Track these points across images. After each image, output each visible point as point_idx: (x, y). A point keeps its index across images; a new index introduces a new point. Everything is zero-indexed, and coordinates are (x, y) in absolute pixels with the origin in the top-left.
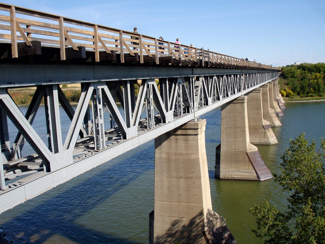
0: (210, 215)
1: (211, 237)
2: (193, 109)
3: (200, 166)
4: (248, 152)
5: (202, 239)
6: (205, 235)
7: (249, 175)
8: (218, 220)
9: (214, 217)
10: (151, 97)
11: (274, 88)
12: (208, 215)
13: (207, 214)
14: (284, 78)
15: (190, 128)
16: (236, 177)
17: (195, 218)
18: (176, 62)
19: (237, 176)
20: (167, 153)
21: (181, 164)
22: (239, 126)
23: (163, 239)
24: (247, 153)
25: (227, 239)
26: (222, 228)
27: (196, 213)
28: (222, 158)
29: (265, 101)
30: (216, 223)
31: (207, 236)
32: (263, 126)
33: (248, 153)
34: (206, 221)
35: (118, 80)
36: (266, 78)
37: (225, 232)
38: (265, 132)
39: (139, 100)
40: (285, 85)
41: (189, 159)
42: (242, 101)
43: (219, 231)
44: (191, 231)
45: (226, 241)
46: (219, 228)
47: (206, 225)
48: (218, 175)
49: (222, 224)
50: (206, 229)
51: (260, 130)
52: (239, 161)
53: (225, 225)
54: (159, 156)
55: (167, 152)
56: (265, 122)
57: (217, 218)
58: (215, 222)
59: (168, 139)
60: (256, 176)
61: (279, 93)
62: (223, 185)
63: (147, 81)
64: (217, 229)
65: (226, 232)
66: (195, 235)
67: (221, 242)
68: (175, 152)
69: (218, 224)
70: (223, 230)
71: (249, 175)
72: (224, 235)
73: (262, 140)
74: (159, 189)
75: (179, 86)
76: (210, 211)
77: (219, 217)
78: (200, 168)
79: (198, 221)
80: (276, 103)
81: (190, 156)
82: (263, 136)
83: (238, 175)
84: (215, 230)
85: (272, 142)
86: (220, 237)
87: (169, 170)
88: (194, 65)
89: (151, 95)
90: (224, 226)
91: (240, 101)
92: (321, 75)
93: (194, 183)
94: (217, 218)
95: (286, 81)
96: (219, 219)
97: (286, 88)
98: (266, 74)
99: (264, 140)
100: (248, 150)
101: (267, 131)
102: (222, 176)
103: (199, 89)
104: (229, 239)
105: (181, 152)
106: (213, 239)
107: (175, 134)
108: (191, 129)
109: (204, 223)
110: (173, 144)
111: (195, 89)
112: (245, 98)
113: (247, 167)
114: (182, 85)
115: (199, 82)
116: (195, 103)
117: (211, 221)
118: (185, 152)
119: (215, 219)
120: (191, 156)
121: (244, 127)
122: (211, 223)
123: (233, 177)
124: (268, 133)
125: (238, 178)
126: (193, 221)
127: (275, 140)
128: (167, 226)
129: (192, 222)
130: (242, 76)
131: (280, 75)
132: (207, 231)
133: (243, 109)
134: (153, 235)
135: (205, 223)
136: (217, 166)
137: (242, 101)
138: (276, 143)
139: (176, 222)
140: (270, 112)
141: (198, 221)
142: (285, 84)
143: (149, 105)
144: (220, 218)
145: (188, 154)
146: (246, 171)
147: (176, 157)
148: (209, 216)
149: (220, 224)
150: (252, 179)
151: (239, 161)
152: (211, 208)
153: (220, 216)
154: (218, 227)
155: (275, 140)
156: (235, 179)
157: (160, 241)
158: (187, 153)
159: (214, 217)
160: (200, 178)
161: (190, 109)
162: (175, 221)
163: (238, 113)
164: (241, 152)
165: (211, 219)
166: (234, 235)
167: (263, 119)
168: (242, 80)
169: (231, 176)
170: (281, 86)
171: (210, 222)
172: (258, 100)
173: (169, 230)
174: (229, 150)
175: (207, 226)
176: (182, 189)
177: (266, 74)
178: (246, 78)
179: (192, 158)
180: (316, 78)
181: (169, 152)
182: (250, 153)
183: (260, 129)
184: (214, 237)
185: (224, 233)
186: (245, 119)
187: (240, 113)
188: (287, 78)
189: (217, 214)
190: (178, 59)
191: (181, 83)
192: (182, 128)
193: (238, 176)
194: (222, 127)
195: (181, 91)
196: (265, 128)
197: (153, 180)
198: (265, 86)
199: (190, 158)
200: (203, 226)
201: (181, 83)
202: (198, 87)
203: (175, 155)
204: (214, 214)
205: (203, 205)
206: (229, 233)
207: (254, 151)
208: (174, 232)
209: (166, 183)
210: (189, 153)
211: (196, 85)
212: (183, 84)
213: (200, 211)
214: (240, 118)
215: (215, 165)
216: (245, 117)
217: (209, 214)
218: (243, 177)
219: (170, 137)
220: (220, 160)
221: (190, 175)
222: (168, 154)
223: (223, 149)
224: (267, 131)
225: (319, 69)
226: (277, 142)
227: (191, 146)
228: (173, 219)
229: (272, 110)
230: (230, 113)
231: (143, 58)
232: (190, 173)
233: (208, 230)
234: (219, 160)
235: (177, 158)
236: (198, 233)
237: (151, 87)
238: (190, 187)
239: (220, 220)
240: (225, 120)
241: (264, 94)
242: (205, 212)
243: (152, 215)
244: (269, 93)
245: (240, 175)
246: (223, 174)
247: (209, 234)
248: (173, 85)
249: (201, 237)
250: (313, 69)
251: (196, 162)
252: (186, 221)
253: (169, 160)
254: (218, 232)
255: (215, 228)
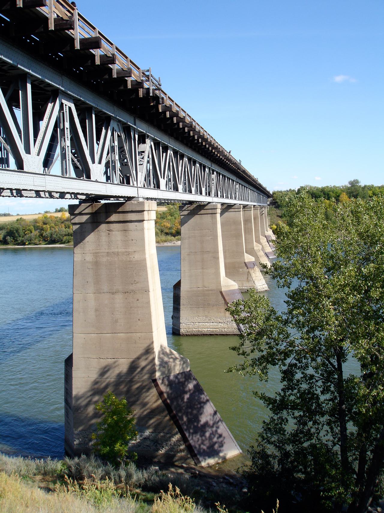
0: (163, 354)
1: (167, 388)
2: (135, 181)
3: (147, 272)
4: (223, 290)
5: (152, 392)
6: (157, 386)
7: (225, 326)
8: (178, 362)
9: (170, 357)
10: (67, 125)
11: (262, 219)
12: (161, 354)
13: (159, 352)
14: (276, 207)
15: (131, 210)
16: (205, 330)
17: (139, 358)
18: (108, 60)
19: (206, 330)
20: (94, 253)
21: (117, 271)
22: (208, 250)
23: (85, 400)
24: (221, 293)
25: (192, 392)
26: (184, 375)
27: (140, 351)
28: (182, 301)
29: (248, 231)
30: (174, 366)
31: (160, 386)
32: (245, 263)
33: (223, 292)
34: (157, 362)
35: (12, 63)
36: (249, 197)
37: (188, 381)
38: (249, 272)
39: (47, 122)
40: (278, 218)
41: (129, 261)
42: (213, 211)
43: (179, 380)
44: (131, 381)
45: (191, 395)
46: (178, 374)
47: (157, 368)
48: (178, 328)
49: (183, 368)
50: (158, 374)
51: (241, 270)
52: (209, 304)
53: (188, 369)
54: (80, 259)
55: (94, 251)
56: (249, 258)
57: (175, 359)
58: (173, 364)
59: (95, 231)
60: (236, 327)
61: (268, 229)
62: (185, 343)
63: (60, 96)
64: (176, 376)
65: (190, 381)
66: (138, 388)
67: (183, 396)
68: (107, 251)
69: (177, 369)
70: (185, 377)
71: (226, 326)
72: (186, 386)
73: (245, 285)
74: (81, 313)
75: (113, 135)
76: (163, 348)
77: (178, 357)
78: (147, 275)
79: (143, 363)
80: (264, 239)
81: (130, 256)
82: (247, 279)
83: (208, 327)
84: (172, 377)
85: (259, 287)
86: (181, 388)
87: (97, 281)
88: (137, 87)
89: (67, 122)
90: (187, 372)
91: (210, 211)
92: (331, 203)
93: (138, 300)
94: (175, 359)
95: (279, 212)
96: (178, 360)
97: (280, 222)
98: (249, 192)
99: (247, 284)
100: (223, 287)
101: (251, 271)
102: (182, 331)
103: (146, 155)
104: (194, 392)
105: (116, 250)
106: (170, 392)
107: (107, 220)
108: (132, 212)
109: (154, 364)
110: (104, 238)
111: (139, 155)
112: (218, 206)
113: (222, 314)
114: (118, 134)
115: (146, 145)
116: (139, 174)
117: (166, 363)
118: (124, 250)
119: (171, 360)
120: (133, 256)
121: (217, 252)
122: (166, 366)
123: (201, 330)
124: (254, 273)
125: (208, 333)
126: (134, 364)
127: (264, 285)
128: (94, 376)
129: (133, 367)
130: (213, 174)
131: (271, 203)
132: (160, 379)
133: (215, 223)
134: (72, 393)
135: (157, 366)
136: (175, 316)
137: (213, 211)
138: (265, 289)
139: (106, 369)
140: (255, 248)
141: (143, 363)
142: (278, 216)
143: (64, 162)
144: (180, 358)
145: (128, 254)
146: (221, 321)
147: (108, 259)
148: (162, 356)
149: (181, 367)
150: (230, 332)
151: (209, 304)
152: (165, 343)
153: (180, 356)
154: (178, 372)
155: (264, 285)
156: (204, 334)
157: (79, 404)
158: (126, 252)
159: (170, 357)
160: (147, 291)
161: (131, 179)
162: (105, 367)
163: (207, 230)
164: (211, 290)
165: (166, 359)
166: (203, 386)
167: (245, 253)
168: (213, 180)
169: (197, 329)
170: (271, 219)
171: (164, 364)
172: (237, 223)
173: (96, 383)
174: (194, 289)
175: (159, 369)
176: (118, 311)
177: (249, 192)
178: (218, 181)
179: (134, 260)
180: (318, 314)
181: (97, 251)
182: (226, 291)
183: (242, 268)
184: (171, 389)
185: (186, 383)
186: (217, 238)
187: (210, 230)
188: (280, 208)
189: (175, 352)
190: (111, 56)
191: (115, 130)
192: (118, 211)
193: (209, 329)
194: (183, 252)
195: (116, 143)
196: (249, 267)
197: (71, 349)
198: (248, 209)
199: (132, 259)
200: (153, 372)
201: (115, 130)
202: (143, 152)
203: (108, 256)
204: (171, 352)
205: (152, 335)
206: (195, 382)
207: (232, 288)
208: (104, 385)
209: (92, 303)
210: (130, 250)
211: (140, 150)
212: (119, 133)
213: (145, 346)
214: (210, 237)
215: (172, 314)
216: (217, 236)
217: (163, 351)
218: (216, 330)
219: (98, 227)
220: (180, 305)
221: (131, 287)
222: (96, 254)
223: (184, 288)
224: (251, 271)
225: (328, 195)
226: (267, 289)
227: (132, 240)
228: (104, 363)
229: (258, 246)
230: (194, 230)
231: (54, 22)
232: (132, 284)
233: (161, 377)
234: (179, 304)
235: (110, 261)
236: (142, 384)
237: (66, 110)
238: (131, 308)
239: (180, 361)
240: (187, 240)
241: (247, 221)
242: (157, 349)
243: (69, 362)
244: (255, 223)
245: (211, 327)
246: (184, 328)
247: (162, 383)
248: (104, 131)
249: (149, 389)
250: (320, 194)
251: (142, 266)
252: (123, 366)
253: (96, 264)
254: (177, 380)
255: (172, 374)
